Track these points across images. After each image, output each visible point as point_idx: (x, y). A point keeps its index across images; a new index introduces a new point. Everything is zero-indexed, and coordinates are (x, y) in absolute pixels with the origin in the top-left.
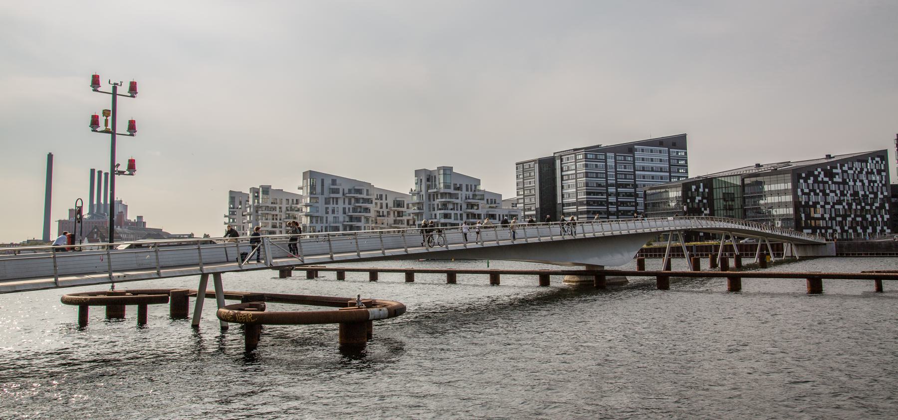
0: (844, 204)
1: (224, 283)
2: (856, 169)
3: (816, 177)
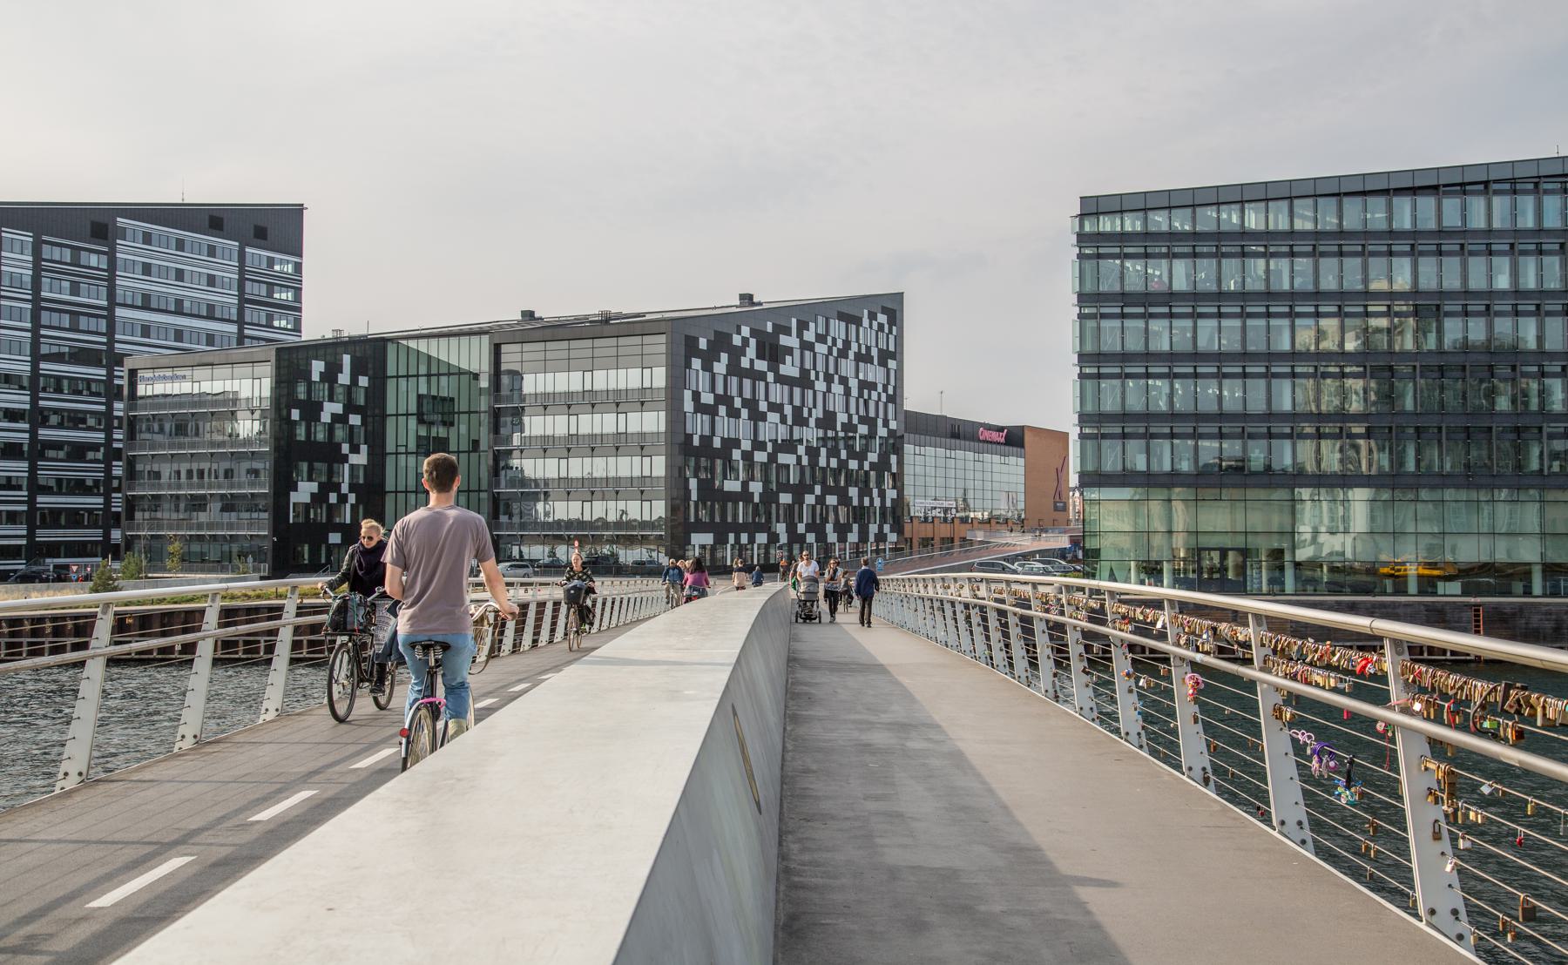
0: (801, 450)
1: (1256, 380)
2: (834, 340)
3: (736, 353)
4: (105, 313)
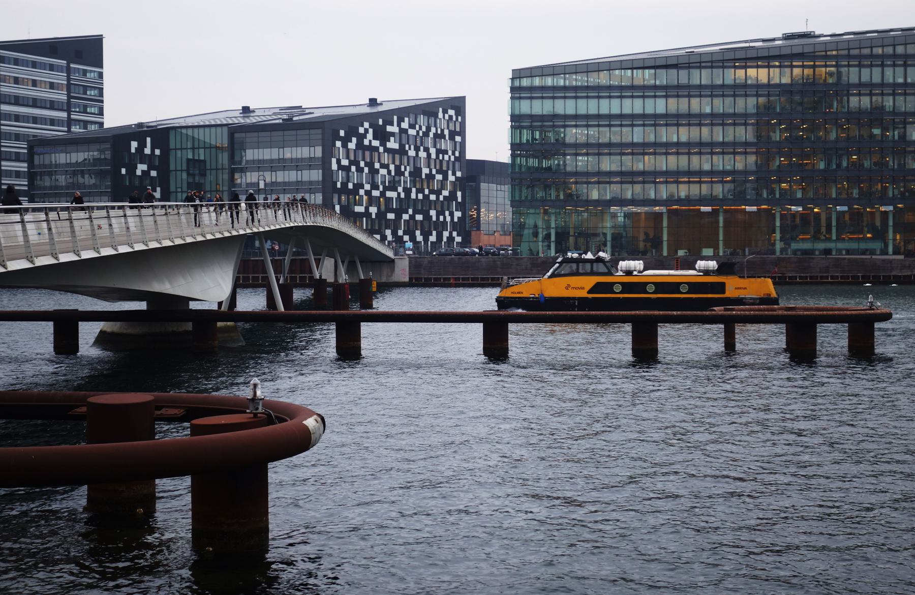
0: (400, 189)
2: (420, 128)
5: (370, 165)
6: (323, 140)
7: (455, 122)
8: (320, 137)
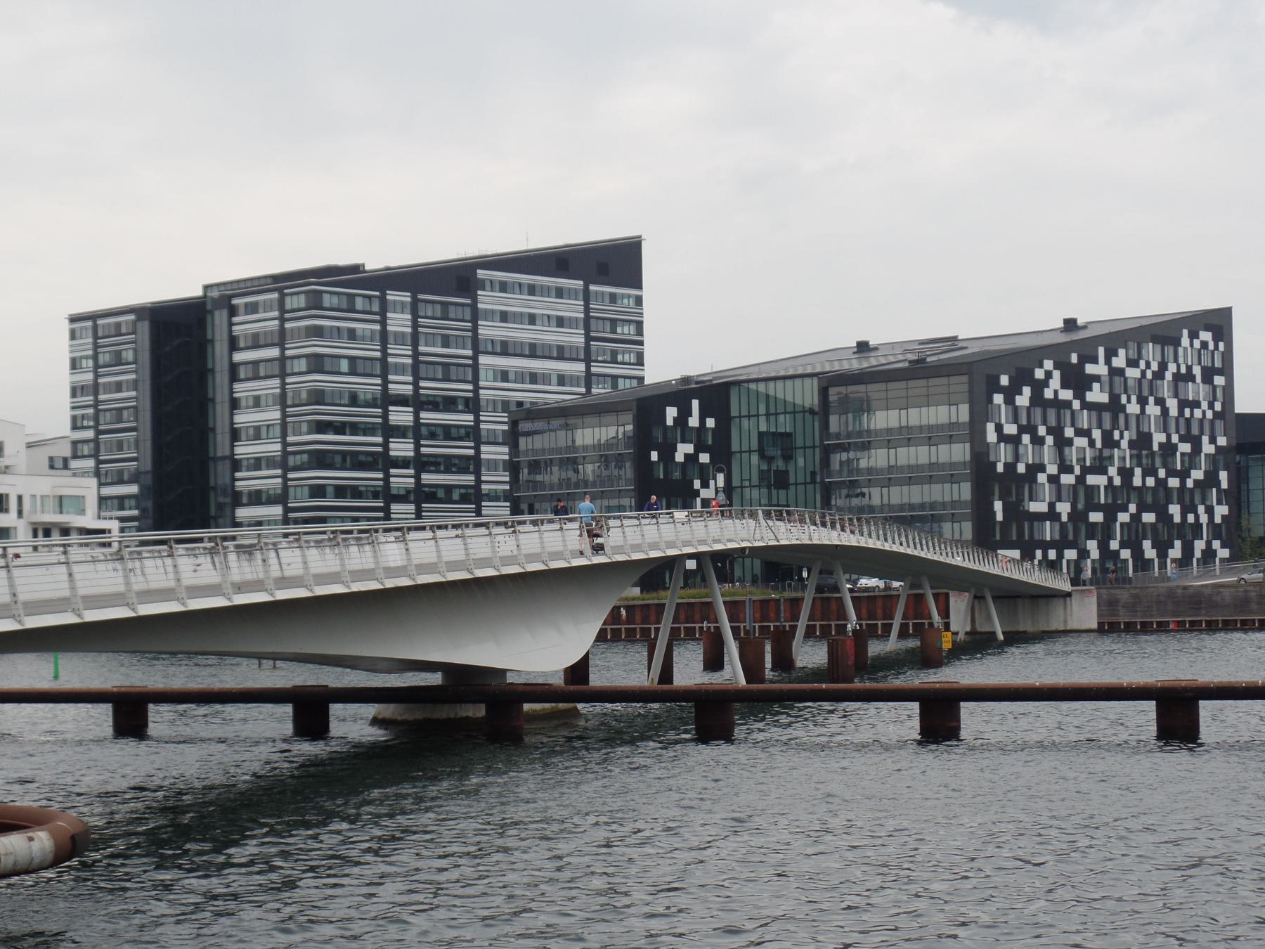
0: (1112, 471)
2: (1148, 365)
4: (470, 362)
5: (1057, 432)
6: (971, 391)
7: (1213, 352)
8: (965, 387)
